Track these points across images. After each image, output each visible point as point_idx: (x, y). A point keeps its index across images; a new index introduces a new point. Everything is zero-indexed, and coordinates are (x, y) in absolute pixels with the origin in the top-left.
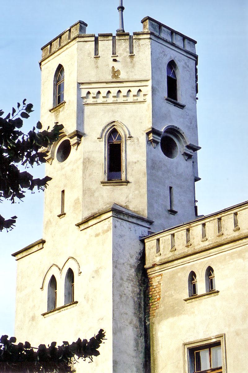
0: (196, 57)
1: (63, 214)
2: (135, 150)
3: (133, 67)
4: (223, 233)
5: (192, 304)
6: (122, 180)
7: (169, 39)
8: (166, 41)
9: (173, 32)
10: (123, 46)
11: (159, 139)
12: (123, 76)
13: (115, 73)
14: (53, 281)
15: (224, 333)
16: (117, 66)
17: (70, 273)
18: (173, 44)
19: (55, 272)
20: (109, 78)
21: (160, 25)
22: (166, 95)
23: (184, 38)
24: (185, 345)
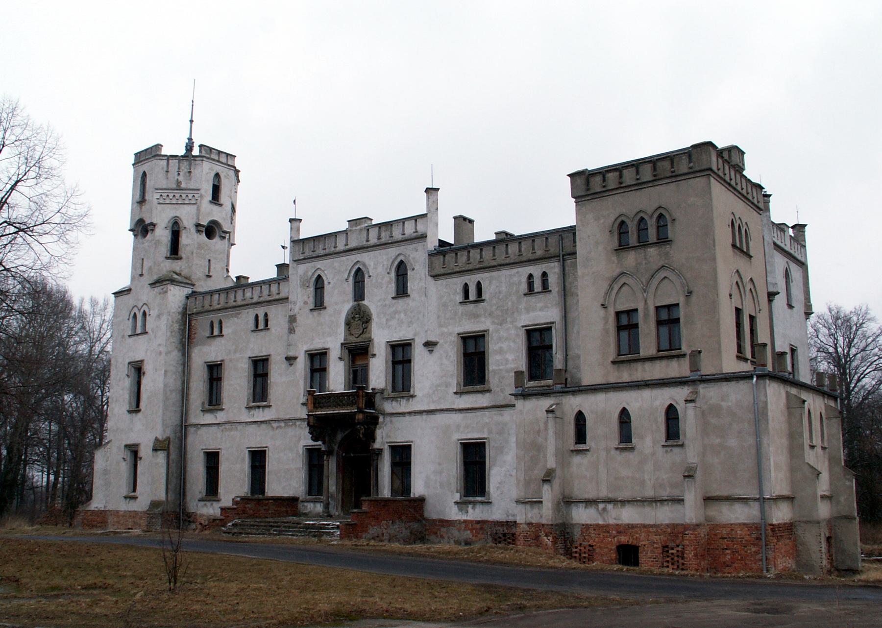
0: (237, 172)
1: (141, 275)
2: (187, 237)
3: (190, 179)
4: (155, 450)
5: (336, 264)
6: (172, 437)
7: (217, 158)
8: (214, 160)
9: (219, 152)
10: (185, 165)
11: (203, 229)
12: (183, 185)
13: (179, 183)
14: (135, 316)
15: (686, 442)
16: (181, 178)
17: (144, 314)
18: (219, 161)
19: (136, 310)
20: (175, 186)
21: (211, 149)
22: (210, 198)
23: (228, 155)
24: (459, 334)
